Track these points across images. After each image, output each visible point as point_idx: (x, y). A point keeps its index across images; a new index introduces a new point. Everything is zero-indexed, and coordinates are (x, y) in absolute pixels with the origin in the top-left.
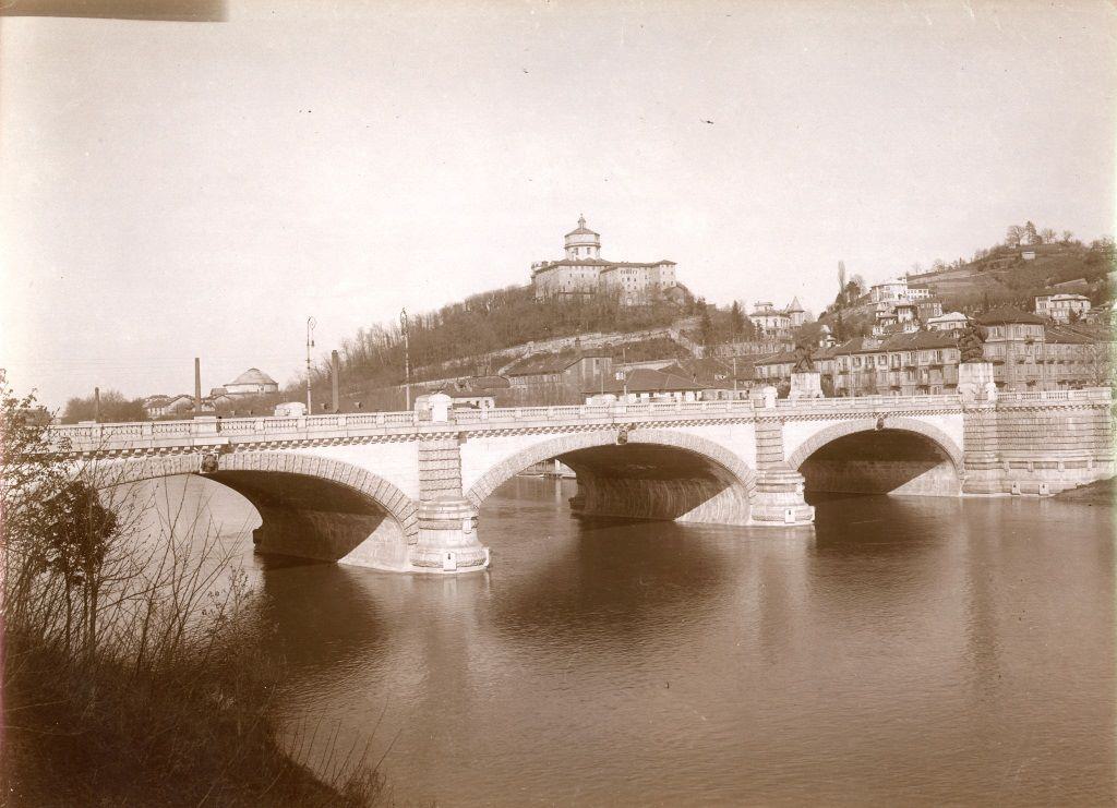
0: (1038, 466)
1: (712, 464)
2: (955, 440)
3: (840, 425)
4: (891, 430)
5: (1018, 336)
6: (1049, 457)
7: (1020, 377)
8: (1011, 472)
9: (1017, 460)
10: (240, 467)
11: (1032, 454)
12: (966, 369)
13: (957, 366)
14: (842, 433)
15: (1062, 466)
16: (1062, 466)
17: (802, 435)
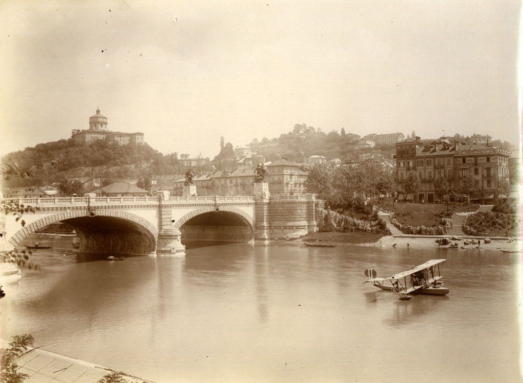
0: (286, 227)
1: (138, 226)
2: (250, 215)
3: (179, 179)
4: (223, 212)
5: (274, 172)
6: (290, 224)
7: (288, 190)
8: (275, 230)
9: (277, 225)
10: (104, 215)
11: (283, 222)
12: (257, 185)
13: (253, 185)
14: (206, 211)
15: (295, 228)
16: (295, 228)
17: (180, 214)
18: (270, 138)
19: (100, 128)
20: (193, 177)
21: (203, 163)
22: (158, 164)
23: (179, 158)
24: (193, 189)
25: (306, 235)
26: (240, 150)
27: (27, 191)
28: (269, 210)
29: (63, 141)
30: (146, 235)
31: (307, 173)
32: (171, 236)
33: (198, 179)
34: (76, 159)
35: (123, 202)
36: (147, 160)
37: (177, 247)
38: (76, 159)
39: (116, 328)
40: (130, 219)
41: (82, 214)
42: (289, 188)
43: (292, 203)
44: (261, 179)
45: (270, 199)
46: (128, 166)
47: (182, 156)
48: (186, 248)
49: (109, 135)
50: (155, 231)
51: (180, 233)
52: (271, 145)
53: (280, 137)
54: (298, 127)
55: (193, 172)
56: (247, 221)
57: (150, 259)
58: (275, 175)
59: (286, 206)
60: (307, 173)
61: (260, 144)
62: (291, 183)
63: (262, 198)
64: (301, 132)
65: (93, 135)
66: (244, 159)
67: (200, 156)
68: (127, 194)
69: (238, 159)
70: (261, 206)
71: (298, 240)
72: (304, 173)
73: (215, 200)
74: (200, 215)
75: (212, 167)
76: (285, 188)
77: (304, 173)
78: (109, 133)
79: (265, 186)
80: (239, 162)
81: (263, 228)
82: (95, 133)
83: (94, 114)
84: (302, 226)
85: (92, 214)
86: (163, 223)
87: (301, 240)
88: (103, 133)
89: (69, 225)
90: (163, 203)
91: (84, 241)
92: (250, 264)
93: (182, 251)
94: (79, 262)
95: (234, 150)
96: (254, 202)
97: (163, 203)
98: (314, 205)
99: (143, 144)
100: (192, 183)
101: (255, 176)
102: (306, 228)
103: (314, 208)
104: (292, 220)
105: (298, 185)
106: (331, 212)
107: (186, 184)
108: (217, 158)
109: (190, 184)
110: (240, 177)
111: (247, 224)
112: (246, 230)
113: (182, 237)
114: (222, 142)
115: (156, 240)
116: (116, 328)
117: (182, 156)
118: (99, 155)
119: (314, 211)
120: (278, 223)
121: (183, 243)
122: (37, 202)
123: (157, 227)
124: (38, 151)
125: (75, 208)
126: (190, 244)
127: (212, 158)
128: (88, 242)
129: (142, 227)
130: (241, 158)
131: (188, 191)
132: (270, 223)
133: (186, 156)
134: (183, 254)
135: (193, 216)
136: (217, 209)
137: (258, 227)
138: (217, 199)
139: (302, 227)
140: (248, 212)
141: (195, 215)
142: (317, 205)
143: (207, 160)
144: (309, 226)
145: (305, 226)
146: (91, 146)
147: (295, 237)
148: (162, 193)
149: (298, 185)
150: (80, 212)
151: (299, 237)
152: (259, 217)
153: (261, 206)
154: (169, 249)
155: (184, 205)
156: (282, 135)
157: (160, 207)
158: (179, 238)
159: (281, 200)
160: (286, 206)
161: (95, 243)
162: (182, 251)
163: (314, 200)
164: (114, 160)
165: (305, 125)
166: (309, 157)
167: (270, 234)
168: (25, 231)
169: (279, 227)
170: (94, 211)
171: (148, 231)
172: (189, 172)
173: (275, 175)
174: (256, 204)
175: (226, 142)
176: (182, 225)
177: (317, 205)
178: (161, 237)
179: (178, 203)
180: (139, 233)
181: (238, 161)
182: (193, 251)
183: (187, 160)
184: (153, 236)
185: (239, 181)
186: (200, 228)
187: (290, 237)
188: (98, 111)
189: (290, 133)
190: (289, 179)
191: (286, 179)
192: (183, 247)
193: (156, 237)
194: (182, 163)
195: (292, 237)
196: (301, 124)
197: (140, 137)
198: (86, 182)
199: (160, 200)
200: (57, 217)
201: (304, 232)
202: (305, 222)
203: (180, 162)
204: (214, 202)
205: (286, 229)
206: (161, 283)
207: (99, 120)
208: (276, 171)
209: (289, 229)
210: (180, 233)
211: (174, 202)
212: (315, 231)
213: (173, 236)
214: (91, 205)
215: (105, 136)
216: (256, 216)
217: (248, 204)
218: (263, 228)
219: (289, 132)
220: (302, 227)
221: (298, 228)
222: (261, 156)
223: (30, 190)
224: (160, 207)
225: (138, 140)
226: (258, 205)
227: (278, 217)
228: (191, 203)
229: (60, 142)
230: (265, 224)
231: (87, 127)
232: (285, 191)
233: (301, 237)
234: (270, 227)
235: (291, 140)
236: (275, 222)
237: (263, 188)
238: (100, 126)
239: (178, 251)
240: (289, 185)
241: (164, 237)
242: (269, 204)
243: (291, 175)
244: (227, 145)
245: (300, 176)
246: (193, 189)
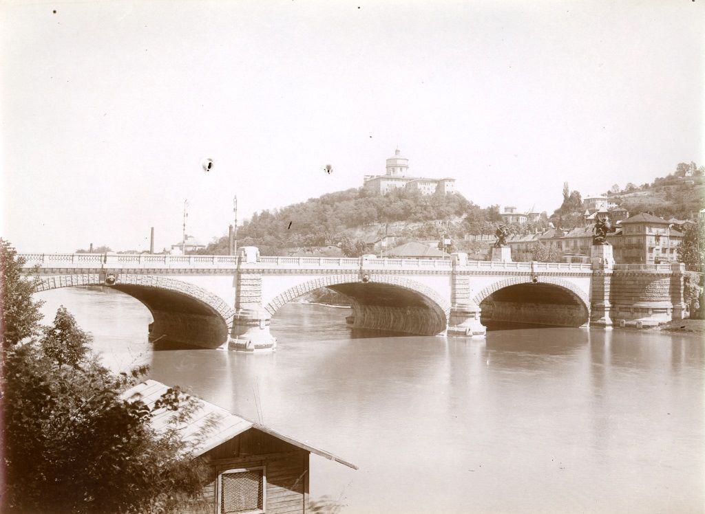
4: (543, 284)
9: (624, 306)
12: (596, 249)
14: (518, 282)
16: (650, 312)
18: (638, 184)
19: (399, 173)
20: (507, 236)
21: (538, 218)
22: (473, 220)
23: (502, 211)
24: (506, 252)
25: (669, 323)
26: (591, 202)
27: (305, 252)
28: (613, 284)
29: (352, 190)
30: (433, 309)
31: (682, 234)
32: (467, 313)
33: (522, 240)
34: (368, 213)
35: (406, 265)
36: (459, 214)
37: (475, 325)
38: (368, 213)
40: (414, 289)
41: (354, 279)
42: (654, 255)
44: (601, 240)
45: (615, 269)
46: (433, 222)
47: (506, 209)
48: (487, 330)
49: (412, 182)
50: (446, 306)
51: (480, 310)
52: (639, 193)
53: (654, 182)
54: (683, 168)
55: (507, 230)
56: (580, 299)
57: (581, 331)
58: (633, 236)
59: (638, 278)
60: (682, 234)
61: (622, 193)
62: (657, 247)
63: (602, 267)
64: (687, 174)
65: (390, 182)
66: (595, 214)
67: (533, 210)
68: (423, 257)
69: (587, 213)
71: (655, 328)
72: (679, 234)
73: (532, 268)
74: (509, 287)
75: (548, 225)
76: (648, 255)
77: (679, 234)
78: (410, 180)
79: (608, 251)
80: (589, 218)
81: (603, 308)
82: (392, 179)
83: (392, 155)
84: (661, 309)
85: (365, 280)
86: (457, 296)
87: (659, 328)
88: (403, 179)
89: (347, 292)
90: (458, 269)
91: (360, 314)
92: (584, 355)
93: (482, 333)
94: (156, 350)
95: (583, 201)
96: (592, 272)
97: (458, 269)
98: (682, 279)
99: (454, 193)
100: (505, 245)
101: (594, 237)
102: (669, 311)
103: (682, 283)
105: (668, 251)
107: (498, 245)
108: (557, 212)
109: (502, 245)
110: (580, 238)
111: (579, 302)
112: (577, 311)
113: (481, 317)
114: (566, 192)
115: (448, 317)
117: (506, 209)
118: (398, 206)
119: (683, 287)
121: (483, 323)
122: (43, 259)
123: (232, 305)
124: (323, 203)
125: (346, 270)
126: (492, 322)
127: (550, 213)
128: (364, 315)
129: (430, 299)
130: (592, 212)
131: (499, 256)
133: (512, 209)
134: (483, 337)
135: (500, 288)
136: (535, 281)
137: (597, 308)
138: (535, 266)
139: (664, 310)
140: (582, 288)
141: (502, 287)
142: (687, 279)
143: (544, 215)
144: (673, 309)
145: (666, 309)
146: (387, 196)
147: (650, 324)
148: (244, 250)
149: (668, 251)
150: (346, 278)
151: (657, 324)
152: (596, 295)
154: (464, 330)
155: (487, 273)
156: (657, 179)
157: (453, 274)
158: (478, 315)
159: (631, 271)
160: (638, 278)
161: (373, 317)
162: (482, 333)
163: (683, 272)
164: (415, 213)
165: (695, 164)
166: (698, 212)
167: (613, 318)
168: (283, 296)
170: (367, 276)
171: (436, 304)
172: (501, 229)
173: (633, 236)
175: (571, 190)
176: (483, 299)
177: (687, 279)
179: (477, 270)
180: (426, 307)
181: (587, 216)
182: (498, 333)
183: (513, 215)
184: (443, 312)
185: (579, 244)
186: (513, 305)
187: (643, 324)
188: (397, 151)
189: (670, 177)
190: (654, 242)
191: (650, 241)
192: (484, 329)
193: (447, 313)
194: (506, 219)
195: (647, 324)
196: (688, 162)
197: (450, 184)
198: (376, 242)
199: (454, 264)
200: (321, 281)
201: (666, 318)
203: (503, 218)
204: (530, 271)
205: (638, 312)
207: (399, 162)
209: (642, 312)
210: (480, 310)
211: (261, 266)
212: (683, 317)
213: (470, 313)
214: (363, 268)
215: (404, 183)
217: (582, 275)
219: (668, 174)
220: (664, 310)
221: (656, 312)
222: (623, 209)
223: (308, 250)
224: (238, 273)
225: (449, 188)
226: (596, 278)
227: (627, 294)
228: (563, 272)
229: (349, 191)
230: (607, 304)
231: (382, 172)
232: (648, 258)
233: (660, 324)
234: (613, 309)
235: (672, 187)
236: (622, 302)
237: (605, 252)
238: (399, 169)
239: (476, 334)
240: (654, 249)
241: (458, 314)
242: (613, 275)
243: (658, 237)
244: (572, 194)
245: (672, 237)
246: (506, 252)
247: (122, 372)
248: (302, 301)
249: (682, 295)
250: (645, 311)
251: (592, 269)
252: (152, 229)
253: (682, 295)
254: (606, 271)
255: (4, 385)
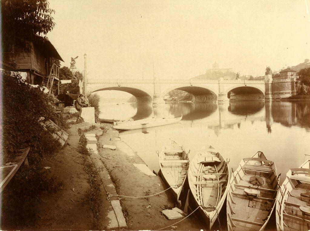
0: (280, 93)
16: (284, 94)
39: (13, 75)
43: (283, 82)
63: (268, 81)
70: (268, 85)
97: (220, 82)
102: (290, 93)
104: (283, 90)
106: (304, 86)
111: (261, 92)
116: (13, 75)
119: (295, 85)
120: (276, 91)
123: (218, 91)
132: (272, 92)
137: (267, 94)
139: (289, 93)
152: (267, 90)
153: (268, 85)
154: (222, 100)
169: (276, 94)
174: (266, 84)
178: (219, 95)
184: (216, 95)
193: (217, 95)
202: (290, 91)
205: (280, 94)
206: (62, 60)
208: (284, 74)
216: (266, 90)
218: (269, 94)
220: (289, 93)
226: (267, 85)
236: (275, 92)
237: (269, 77)
242: (272, 84)
247: (146, 134)
248: (265, 205)
249: (295, 88)
250: (282, 93)
251: (265, 82)
252: (190, 151)
253: (295, 88)
254: (269, 82)
255: (47, 25)
